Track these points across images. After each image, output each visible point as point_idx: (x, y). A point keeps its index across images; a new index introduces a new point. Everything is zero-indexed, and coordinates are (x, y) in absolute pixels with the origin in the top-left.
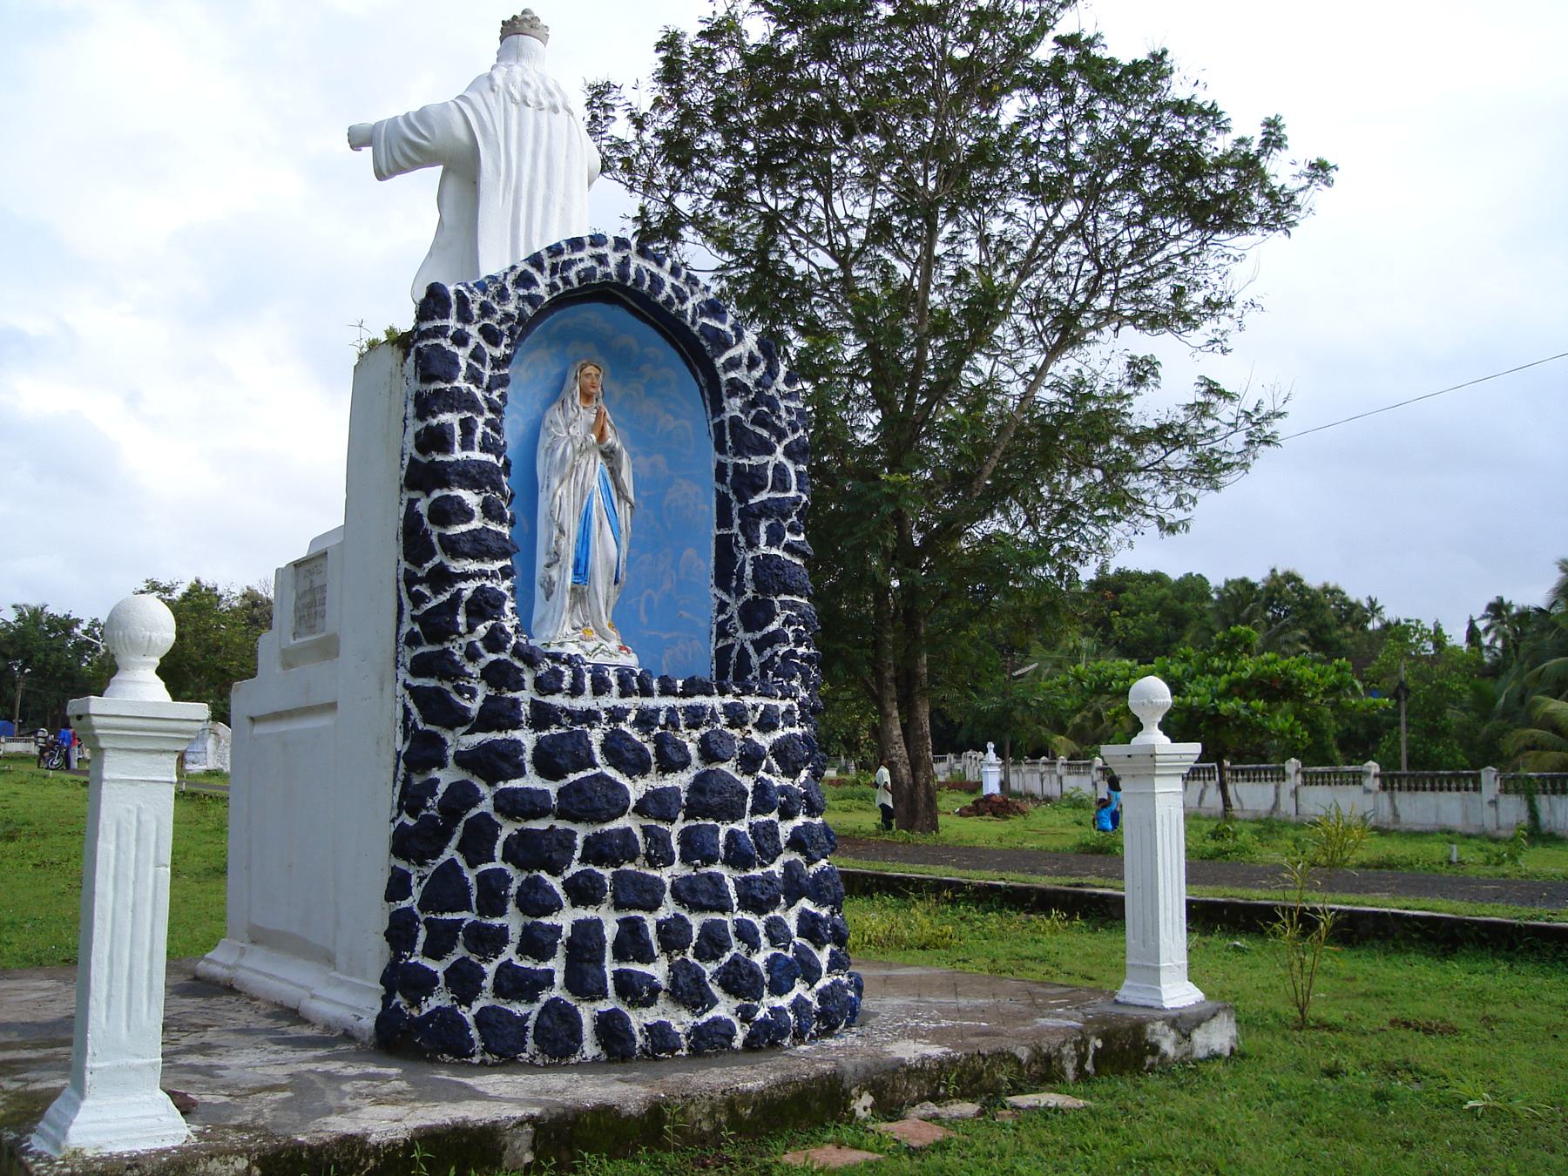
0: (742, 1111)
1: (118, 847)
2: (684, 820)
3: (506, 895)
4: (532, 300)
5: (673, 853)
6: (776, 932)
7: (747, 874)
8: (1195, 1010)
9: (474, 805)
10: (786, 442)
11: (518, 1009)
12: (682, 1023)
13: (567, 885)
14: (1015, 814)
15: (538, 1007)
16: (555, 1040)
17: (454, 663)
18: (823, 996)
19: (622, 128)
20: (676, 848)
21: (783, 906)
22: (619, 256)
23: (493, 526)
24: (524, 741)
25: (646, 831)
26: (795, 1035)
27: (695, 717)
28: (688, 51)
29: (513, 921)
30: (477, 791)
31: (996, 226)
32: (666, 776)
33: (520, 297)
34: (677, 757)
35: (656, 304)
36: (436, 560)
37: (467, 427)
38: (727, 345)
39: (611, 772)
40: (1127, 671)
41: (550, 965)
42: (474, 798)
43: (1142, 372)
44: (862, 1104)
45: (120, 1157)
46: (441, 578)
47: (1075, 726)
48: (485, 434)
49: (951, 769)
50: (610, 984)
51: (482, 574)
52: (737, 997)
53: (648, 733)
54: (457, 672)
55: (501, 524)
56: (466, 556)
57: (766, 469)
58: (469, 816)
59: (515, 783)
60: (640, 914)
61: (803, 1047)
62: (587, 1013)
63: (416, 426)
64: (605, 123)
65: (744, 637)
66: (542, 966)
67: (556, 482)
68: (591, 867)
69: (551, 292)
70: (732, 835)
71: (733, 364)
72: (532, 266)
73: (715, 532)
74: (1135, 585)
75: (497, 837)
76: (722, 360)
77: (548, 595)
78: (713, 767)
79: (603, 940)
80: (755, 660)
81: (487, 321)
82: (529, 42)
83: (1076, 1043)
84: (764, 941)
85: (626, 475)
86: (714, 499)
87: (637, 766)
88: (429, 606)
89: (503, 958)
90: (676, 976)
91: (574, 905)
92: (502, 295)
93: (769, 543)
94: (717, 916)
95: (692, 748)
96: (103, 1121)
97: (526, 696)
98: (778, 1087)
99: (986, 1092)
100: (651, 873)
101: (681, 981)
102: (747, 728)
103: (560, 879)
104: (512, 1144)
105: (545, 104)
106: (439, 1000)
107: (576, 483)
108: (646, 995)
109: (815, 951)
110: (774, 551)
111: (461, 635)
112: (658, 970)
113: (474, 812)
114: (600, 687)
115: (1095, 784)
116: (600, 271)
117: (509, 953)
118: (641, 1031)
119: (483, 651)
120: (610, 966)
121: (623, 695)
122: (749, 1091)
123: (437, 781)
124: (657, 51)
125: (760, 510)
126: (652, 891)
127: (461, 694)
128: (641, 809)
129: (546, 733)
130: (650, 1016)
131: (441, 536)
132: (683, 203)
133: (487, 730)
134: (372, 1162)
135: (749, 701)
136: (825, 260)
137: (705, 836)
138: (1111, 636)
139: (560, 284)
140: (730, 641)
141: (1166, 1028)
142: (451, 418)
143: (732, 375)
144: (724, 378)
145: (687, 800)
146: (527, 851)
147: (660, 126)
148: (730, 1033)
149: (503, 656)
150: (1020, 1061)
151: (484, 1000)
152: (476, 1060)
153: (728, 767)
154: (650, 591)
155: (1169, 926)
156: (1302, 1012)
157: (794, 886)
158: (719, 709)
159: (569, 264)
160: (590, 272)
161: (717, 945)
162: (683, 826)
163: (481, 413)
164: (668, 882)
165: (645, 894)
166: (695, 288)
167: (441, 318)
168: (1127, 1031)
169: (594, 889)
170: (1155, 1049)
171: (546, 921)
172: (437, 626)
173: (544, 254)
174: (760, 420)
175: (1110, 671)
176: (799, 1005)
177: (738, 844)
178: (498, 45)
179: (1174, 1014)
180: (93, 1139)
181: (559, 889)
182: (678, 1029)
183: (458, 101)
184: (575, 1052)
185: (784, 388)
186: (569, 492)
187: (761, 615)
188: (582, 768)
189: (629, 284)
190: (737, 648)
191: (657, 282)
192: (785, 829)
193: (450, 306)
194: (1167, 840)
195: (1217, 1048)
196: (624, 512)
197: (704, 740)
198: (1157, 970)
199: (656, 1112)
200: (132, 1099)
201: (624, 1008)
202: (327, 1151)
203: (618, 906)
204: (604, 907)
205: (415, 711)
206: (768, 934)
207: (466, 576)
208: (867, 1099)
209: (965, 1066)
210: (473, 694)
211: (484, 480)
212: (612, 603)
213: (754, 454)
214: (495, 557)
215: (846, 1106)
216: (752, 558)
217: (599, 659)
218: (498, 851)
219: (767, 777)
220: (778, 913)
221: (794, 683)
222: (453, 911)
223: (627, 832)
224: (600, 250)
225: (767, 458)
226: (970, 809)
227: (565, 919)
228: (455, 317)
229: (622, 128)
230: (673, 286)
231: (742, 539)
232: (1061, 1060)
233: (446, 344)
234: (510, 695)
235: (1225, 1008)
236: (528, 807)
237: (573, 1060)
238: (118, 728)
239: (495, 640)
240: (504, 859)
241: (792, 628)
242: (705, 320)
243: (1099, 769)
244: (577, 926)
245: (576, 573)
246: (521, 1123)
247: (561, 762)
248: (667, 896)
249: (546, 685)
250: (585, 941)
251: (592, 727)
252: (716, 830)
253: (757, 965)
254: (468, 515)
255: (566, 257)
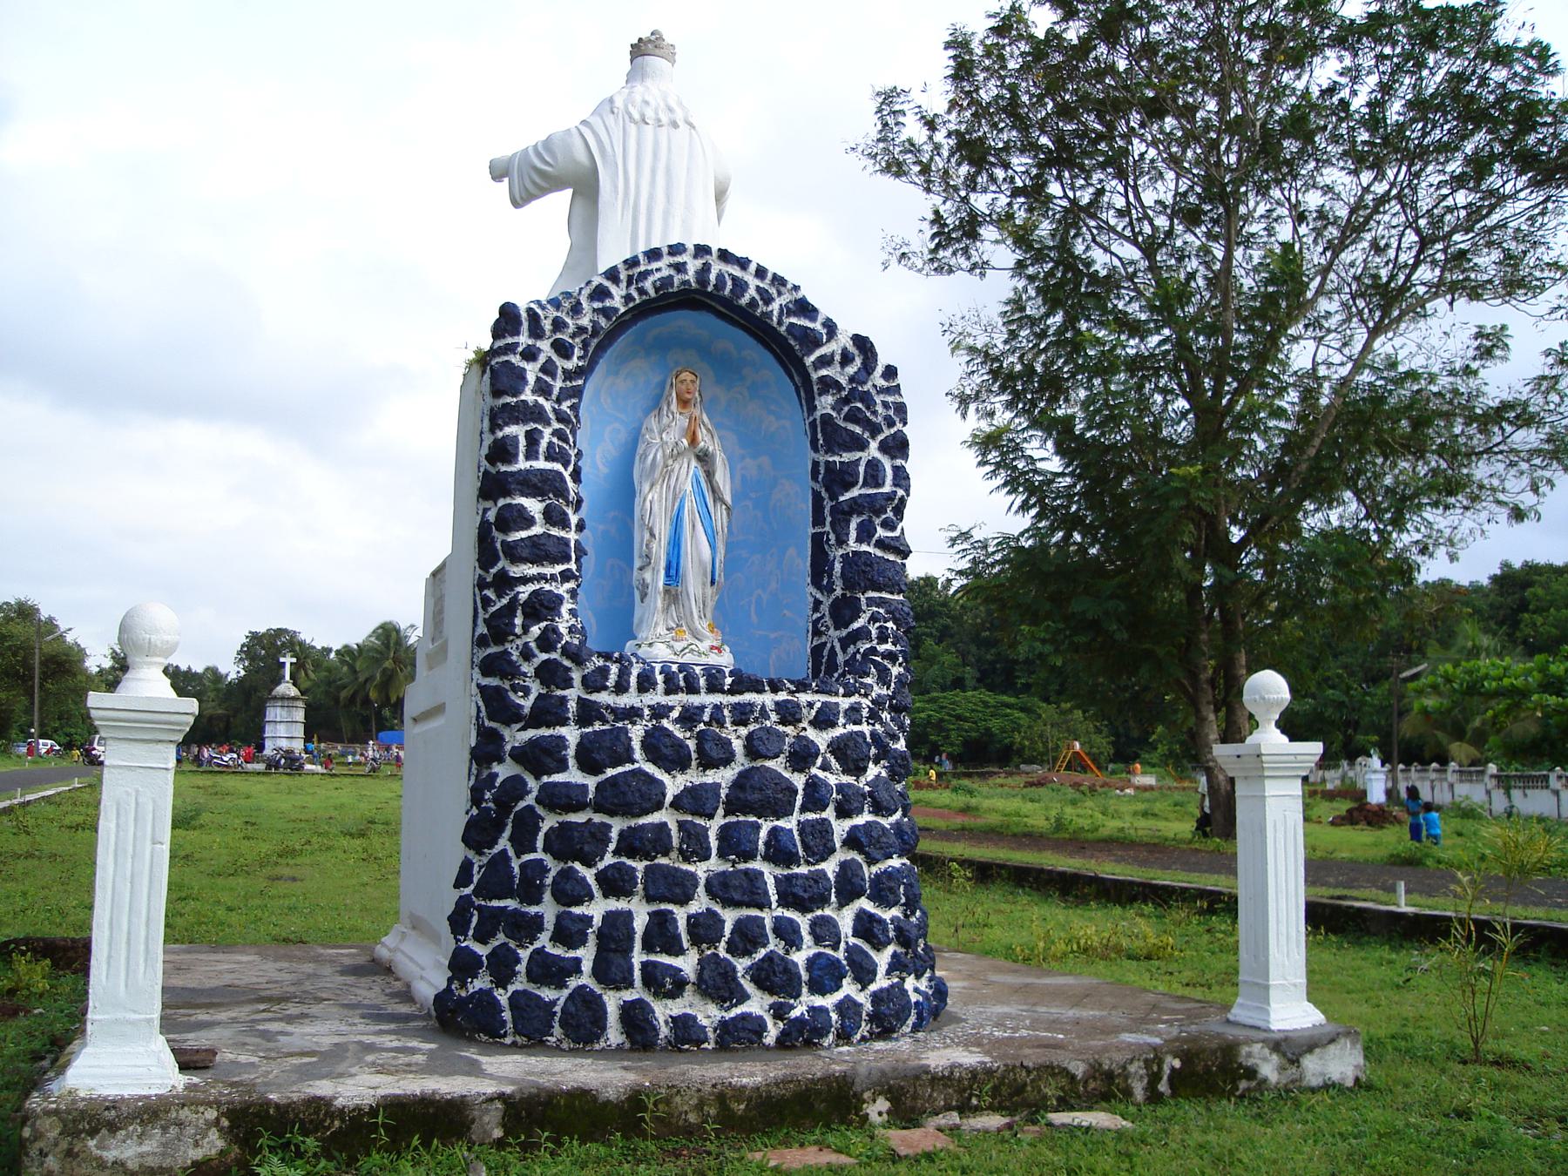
0: (734, 1106)
1: (118, 825)
2: (725, 816)
3: (542, 885)
4: (606, 312)
5: (709, 849)
6: (825, 931)
7: (790, 872)
8: (1306, 1034)
9: (522, 798)
10: (881, 437)
11: (547, 994)
12: (709, 1017)
13: (600, 877)
14: (1391, 823)
15: (566, 993)
16: (578, 1026)
17: (511, 663)
18: (877, 998)
19: (913, 130)
20: (714, 843)
21: (834, 905)
22: (699, 263)
23: (555, 532)
24: (568, 737)
25: (682, 825)
26: (839, 1036)
27: (742, 714)
28: (979, 51)
29: (548, 909)
30: (525, 784)
31: (1313, 200)
32: (708, 772)
33: (594, 310)
34: (715, 753)
35: (740, 307)
36: (500, 565)
37: (533, 439)
38: (818, 344)
39: (650, 768)
40: (1501, 670)
41: (579, 953)
42: (523, 791)
43: (1490, 344)
44: (877, 1109)
45: (105, 1099)
46: (504, 583)
47: (1475, 730)
48: (550, 444)
49: (1343, 778)
50: (637, 974)
51: (541, 577)
52: (772, 993)
53: (691, 730)
54: (515, 672)
55: (563, 529)
56: (524, 560)
57: (858, 465)
58: (517, 809)
59: (558, 778)
60: (670, 907)
61: (845, 1048)
62: (612, 1002)
63: (488, 440)
64: (895, 130)
65: (834, 635)
66: (572, 954)
67: (646, 487)
68: (624, 859)
69: (626, 303)
70: (774, 832)
71: (825, 361)
72: (608, 279)
73: (811, 530)
74: (1543, 579)
75: (539, 829)
76: (812, 358)
77: (644, 596)
78: (758, 763)
79: (632, 932)
80: (841, 658)
81: (559, 336)
82: (654, 62)
83: (1146, 1061)
84: (807, 939)
85: (722, 477)
86: (810, 498)
87: (675, 760)
88: (494, 609)
89: (537, 945)
90: (702, 969)
91: (606, 896)
92: (576, 310)
93: (859, 540)
94: (754, 912)
95: (738, 745)
96: (99, 1066)
97: (573, 694)
98: (777, 1084)
99: (1029, 1106)
100: (685, 867)
101: (706, 975)
102: (801, 725)
103: (594, 871)
104: (481, 1118)
105: (665, 120)
106: (481, 983)
107: (668, 487)
108: (669, 986)
109: (872, 953)
110: (864, 548)
111: (519, 637)
112: (687, 963)
113: (522, 804)
114: (646, 684)
115: (1488, 792)
116: (677, 279)
117: (544, 940)
118: (666, 1022)
119: (536, 651)
120: (638, 957)
121: (668, 692)
122: (744, 1087)
123: (496, 775)
124: (946, 48)
125: (851, 507)
126: (682, 885)
127: (516, 693)
128: (677, 804)
129: (590, 729)
130: (676, 1007)
131: (503, 542)
132: (980, 202)
133: (537, 727)
134: (337, 1123)
135: (804, 698)
136: (1130, 252)
137: (743, 833)
138: (1518, 634)
139: (635, 295)
140: (824, 639)
141: (1267, 1051)
142: (517, 431)
143: (824, 372)
144: (814, 376)
145: (727, 796)
146: (568, 844)
147: (952, 127)
148: (761, 1028)
149: (554, 656)
150: (1073, 1077)
151: (520, 984)
152: (508, 1040)
153: (777, 765)
154: (759, 591)
155: (1283, 940)
156: (1476, 1042)
157: (849, 887)
158: (770, 705)
159: (644, 275)
160: (667, 281)
161: (750, 941)
162: (723, 822)
163: (548, 423)
164: (702, 876)
165: (681, 889)
166: (782, 289)
167: (512, 335)
168: (1214, 1052)
169: (623, 881)
170: (1251, 1073)
171: (577, 910)
172: (498, 629)
173: (621, 268)
174: (853, 417)
175: (1483, 671)
176: (847, 1008)
177: (778, 841)
178: (628, 67)
179: (1278, 1036)
180: (88, 1081)
181: (591, 880)
182: (705, 1022)
183: (581, 127)
184: (598, 1039)
185: (881, 383)
186: (661, 496)
187: (847, 613)
188: (620, 763)
189: (710, 289)
190: (829, 645)
191: (740, 285)
192: (840, 828)
193: (520, 323)
194: (1281, 853)
195: (1336, 1077)
196: (720, 516)
197: (750, 737)
198: (1267, 988)
199: (635, 1100)
200: (127, 1049)
201: (649, 999)
202: (293, 1109)
203: (649, 899)
204: (636, 899)
205: (483, 709)
206: (813, 932)
207: (525, 580)
208: (883, 1104)
209: (1003, 1077)
210: (527, 691)
211: (547, 488)
212: (710, 604)
213: (845, 451)
214: (555, 561)
215: (858, 1109)
216: (842, 556)
217: (688, 659)
218: (540, 844)
219: (821, 774)
220: (828, 912)
221: (868, 680)
222: (500, 898)
223: (663, 826)
224: (679, 259)
225: (858, 454)
226: (1343, 818)
227: (597, 909)
228: (526, 334)
229: (913, 130)
230: (758, 289)
231: (832, 537)
232: (1126, 1078)
233: (515, 359)
234: (559, 693)
235: (1348, 1034)
236: (564, 801)
237: (597, 1047)
238: (114, 720)
239: (547, 641)
240: (545, 850)
241: (877, 625)
242: (794, 320)
243: (1492, 776)
244: (609, 917)
245: (668, 575)
246: (491, 1100)
247: (598, 757)
248: (701, 890)
249: (594, 682)
250: (615, 932)
251: (634, 723)
252: (758, 827)
253: (796, 965)
254: (529, 522)
255: (642, 268)
